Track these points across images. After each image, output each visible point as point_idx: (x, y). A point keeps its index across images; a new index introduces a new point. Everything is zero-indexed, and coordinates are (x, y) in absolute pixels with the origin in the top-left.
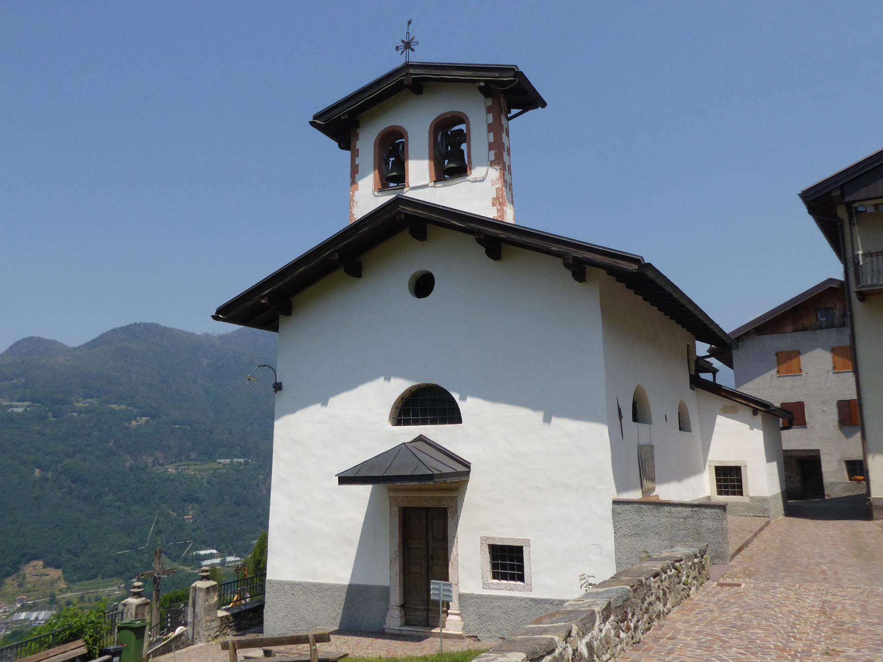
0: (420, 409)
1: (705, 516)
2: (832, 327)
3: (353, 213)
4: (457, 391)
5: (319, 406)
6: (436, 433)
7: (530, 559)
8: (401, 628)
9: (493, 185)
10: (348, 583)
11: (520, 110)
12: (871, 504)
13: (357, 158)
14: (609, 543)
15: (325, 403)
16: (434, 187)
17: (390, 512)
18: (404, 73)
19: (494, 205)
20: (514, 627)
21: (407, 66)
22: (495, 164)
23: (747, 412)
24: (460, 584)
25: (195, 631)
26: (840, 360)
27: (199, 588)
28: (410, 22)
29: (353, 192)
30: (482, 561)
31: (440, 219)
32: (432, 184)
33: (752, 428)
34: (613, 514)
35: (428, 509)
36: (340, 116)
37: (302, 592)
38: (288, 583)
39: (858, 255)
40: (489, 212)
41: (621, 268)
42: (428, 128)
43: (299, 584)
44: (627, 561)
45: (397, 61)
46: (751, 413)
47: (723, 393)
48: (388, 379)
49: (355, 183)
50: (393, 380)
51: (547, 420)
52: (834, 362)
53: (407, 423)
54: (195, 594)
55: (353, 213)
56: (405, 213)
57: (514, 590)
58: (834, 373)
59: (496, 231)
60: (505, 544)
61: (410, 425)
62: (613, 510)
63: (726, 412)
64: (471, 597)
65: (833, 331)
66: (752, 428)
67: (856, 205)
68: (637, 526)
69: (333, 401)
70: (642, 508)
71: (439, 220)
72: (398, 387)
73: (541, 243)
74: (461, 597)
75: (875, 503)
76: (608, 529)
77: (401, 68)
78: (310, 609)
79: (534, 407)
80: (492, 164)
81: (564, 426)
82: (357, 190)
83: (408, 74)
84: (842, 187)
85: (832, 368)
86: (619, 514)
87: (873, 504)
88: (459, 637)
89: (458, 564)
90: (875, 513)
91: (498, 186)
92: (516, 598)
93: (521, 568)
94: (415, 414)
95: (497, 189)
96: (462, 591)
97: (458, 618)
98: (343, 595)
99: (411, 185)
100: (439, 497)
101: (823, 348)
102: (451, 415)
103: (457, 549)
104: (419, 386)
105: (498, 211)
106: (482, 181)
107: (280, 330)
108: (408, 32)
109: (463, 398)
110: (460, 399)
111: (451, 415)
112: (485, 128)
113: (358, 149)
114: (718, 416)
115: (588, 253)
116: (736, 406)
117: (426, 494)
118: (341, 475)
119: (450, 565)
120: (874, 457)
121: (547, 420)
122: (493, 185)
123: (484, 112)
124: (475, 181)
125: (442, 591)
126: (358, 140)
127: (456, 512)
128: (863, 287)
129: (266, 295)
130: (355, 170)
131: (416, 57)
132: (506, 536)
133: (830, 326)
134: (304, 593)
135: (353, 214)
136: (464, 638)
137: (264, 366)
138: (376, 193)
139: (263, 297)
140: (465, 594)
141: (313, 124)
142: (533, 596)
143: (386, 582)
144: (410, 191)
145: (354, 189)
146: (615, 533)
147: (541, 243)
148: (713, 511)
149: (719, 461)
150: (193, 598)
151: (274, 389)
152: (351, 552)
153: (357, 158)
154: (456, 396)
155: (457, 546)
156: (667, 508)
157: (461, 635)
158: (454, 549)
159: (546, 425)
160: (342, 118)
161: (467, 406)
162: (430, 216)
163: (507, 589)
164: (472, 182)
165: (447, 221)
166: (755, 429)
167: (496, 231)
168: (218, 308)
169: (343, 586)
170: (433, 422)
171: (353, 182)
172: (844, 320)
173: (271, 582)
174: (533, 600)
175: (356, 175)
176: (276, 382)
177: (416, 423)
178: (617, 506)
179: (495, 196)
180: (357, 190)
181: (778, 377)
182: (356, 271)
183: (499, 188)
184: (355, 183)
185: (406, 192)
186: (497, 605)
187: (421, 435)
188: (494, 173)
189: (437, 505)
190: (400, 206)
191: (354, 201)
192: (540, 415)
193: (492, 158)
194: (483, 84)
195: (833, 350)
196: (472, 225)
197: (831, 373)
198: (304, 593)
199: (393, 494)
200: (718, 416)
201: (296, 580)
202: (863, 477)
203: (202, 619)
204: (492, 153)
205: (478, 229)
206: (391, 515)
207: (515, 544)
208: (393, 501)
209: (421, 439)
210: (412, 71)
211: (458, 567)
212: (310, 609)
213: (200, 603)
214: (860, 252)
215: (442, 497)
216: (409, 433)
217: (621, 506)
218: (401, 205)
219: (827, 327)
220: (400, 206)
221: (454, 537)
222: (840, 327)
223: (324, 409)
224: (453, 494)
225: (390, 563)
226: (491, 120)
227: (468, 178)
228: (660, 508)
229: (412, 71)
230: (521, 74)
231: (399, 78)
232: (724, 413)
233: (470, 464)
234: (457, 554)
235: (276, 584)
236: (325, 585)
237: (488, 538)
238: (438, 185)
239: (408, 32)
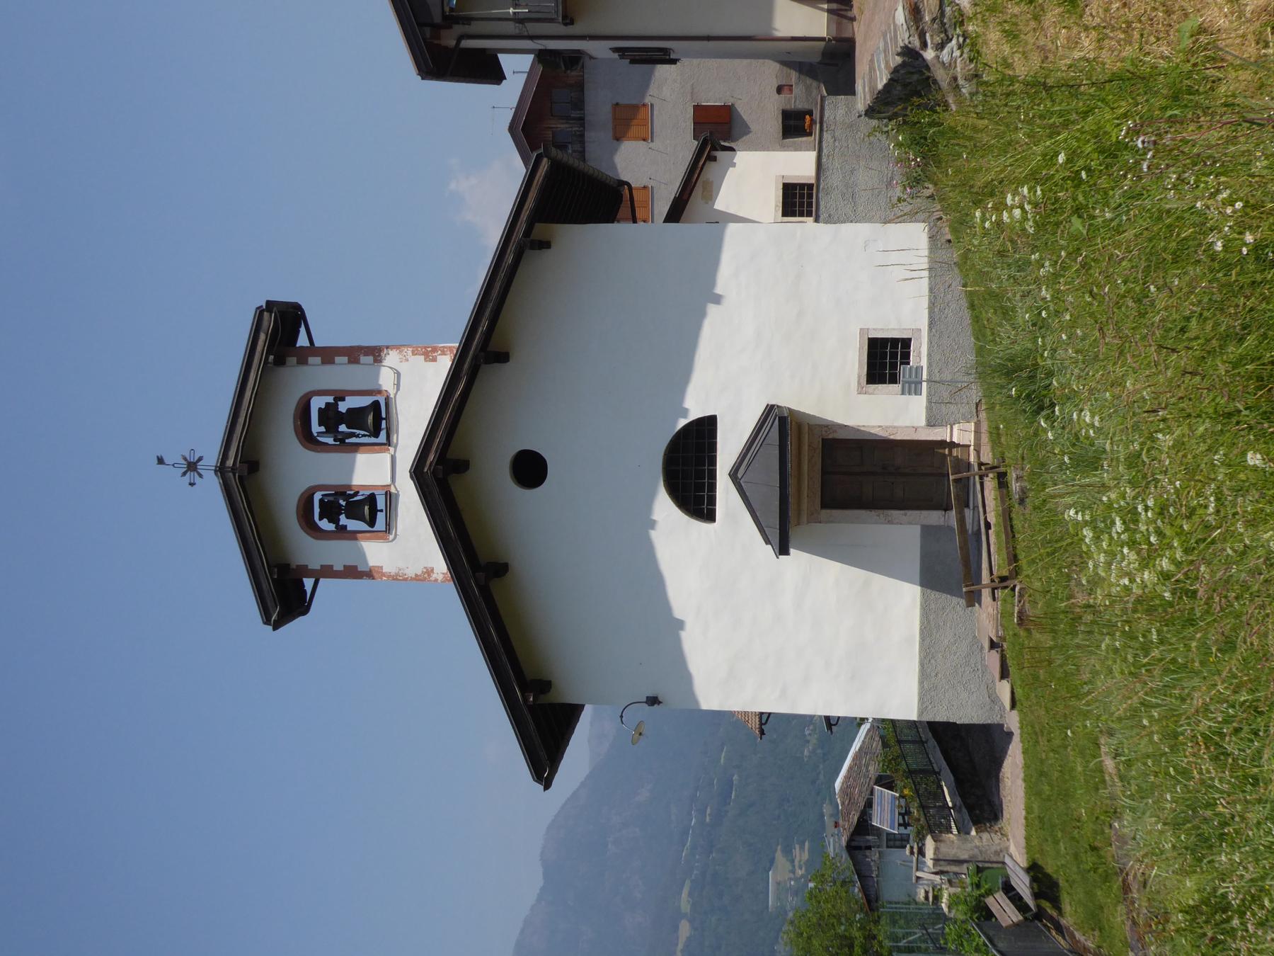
0: (695, 479)
1: (832, 118)
2: (582, 136)
3: (414, 576)
4: (675, 422)
5: (683, 634)
6: (728, 450)
7: (882, 329)
8: (971, 508)
9: (407, 360)
10: (919, 588)
11: (303, 325)
12: (835, 39)
13: (335, 569)
14: (862, 230)
15: (680, 624)
16: (396, 447)
17: (826, 522)
18: (231, 474)
19: (434, 360)
20: (962, 353)
21: (221, 470)
22: (380, 355)
23: (711, 170)
24: (915, 425)
25: (995, 860)
26: (634, 130)
27: (935, 854)
28: (161, 461)
29: (383, 574)
30: (886, 395)
31: (451, 413)
32: (392, 449)
33: (734, 165)
34: (830, 223)
35: (824, 472)
36: (273, 579)
37: (933, 661)
38: (921, 683)
39: (514, 13)
40: (445, 364)
41: (544, 180)
42: (313, 453)
43: (922, 665)
44: (883, 208)
45: (211, 485)
46: (713, 163)
47: (685, 197)
48: (652, 524)
49: (370, 571)
50: (655, 517)
51: (717, 300)
52: (636, 139)
53: (712, 501)
54: (944, 860)
55: (414, 576)
56: (436, 464)
57: (920, 352)
58: (652, 141)
59: (479, 334)
60: (866, 361)
61: (716, 470)
62: (826, 223)
63: (710, 195)
64: (929, 409)
65: (590, 135)
66: (734, 165)
67: (447, 9)
68: (843, 195)
69: (678, 613)
70: (823, 189)
71: (453, 414)
72: (665, 508)
73: (501, 275)
74: (931, 423)
75: (834, 33)
76: (847, 229)
77: (223, 479)
78: (954, 648)
79: (702, 315)
80: (378, 360)
81: (725, 279)
82: (382, 567)
83: (233, 469)
84: (420, 25)
85: (645, 143)
86: (830, 216)
87: (834, 36)
88: (978, 425)
89: (891, 427)
90: (847, 35)
91: (410, 353)
92: (929, 349)
93: (894, 342)
94: (700, 487)
95: (414, 353)
96: (923, 422)
97: (956, 427)
98: (934, 595)
99: (388, 481)
100: (809, 450)
101: (615, 150)
102: (705, 429)
103: (873, 427)
104: (664, 481)
105: (443, 353)
106: (398, 374)
107: (574, 700)
108: (173, 465)
109: (685, 412)
110: (685, 417)
111: (705, 429)
112: (328, 368)
113: (321, 566)
114: (716, 207)
115: (522, 216)
116: (704, 182)
117: (805, 467)
118: (777, 551)
119: (892, 437)
120: (776, 30)
121: (717, 300)
122: (407, 360)
123: (305, 368)
124: (398, 385)
125: (912, 380)
126: (307, 566)
127: (827, 426)
128: (557, 12)
129: (523, 695)
130: (352, 572)
131: (211, 454)
132: (855, 361)
133: (581, 138)
134: (933, 657)
135: (416, 575)
136: (979, 421)
137: (622, 717)
138: (391, 537)
139: (525, 699)
140: (926, 418)
141: (276, 626)
142: (927, 328)
143: (916, 531)
144: (396, 484)
145: (378, 572)
146: (851, 222)
147: (501, 275)
148: (826, 108)
149: (776, 211)
150: (949, 864)
151: (656, 706)
152: (879, 581)
153: (335, 569)
154: (682, 423)
155: (868, 426)
156: (824, 160)
157: (975, 423)
158: (873, 431)
159: (725, 302)
160: (276, 577)
161: (695, 409)
162: (445, 428)
163: (920, 355)
164: (398, 389)
165: (456, 401)
166: (735, 161)
167: (479, 334)
168: (534, 780)
169: (923, 594)
170: (713, 461)
171: (369, 574)
172: (574, 119)
173: (921, 713)
174: (930, 328)
175: (359, 570)
176: (646, 702)
177: (712, 487)
178: (822, 217)
179: (423, 357)
180: (382, 567)
181: (652, 222)
182: (501, 569)
183: (413, 352)
184: (370, 571)
185: (397, 490)
186: (938, 375)
187: (729, 474)
188: (391, 358)
189: (819, 451)
190: (426, 470)
191: (397, 575)
192: (712, 309)
193: (370, 359)
194: (271, 357)
195: (618, 138)
196: (466, 366)
197: (651, 145)
198: (933, 657)
199: (804, 518)
200: (716, 207)
201: (917, 670)
202: (807, 117)
203: (977, 847)
204: (363, 359)
205: (472, 360)
206: (832, 522)
207: (866, 347)
208: (813, 519)
209: (734, 475)
210: (230, 463)
211: (895, 427)
212: (954, 648)
213: (954, 851)
214: (511, 10)
215: (809, 446)
216: (726, 494)
217: (821, 212)
218: (423, 468)
219: (583, 143)
220: (426, 470)
221: (858, 430)
222: (583, 125)
223: (688, 626)
224: (806, 429)
225: (892, 524)
226: (318, 360)
227: (392, 396)
228: (824, 167)
229: (230, 463)
230: (270, 304)
231: (234, 483)
232: (711, 200)
233: (768, 405)
234: (879, 427)
235: (923, 703)
236: (922, 623)
237: (859, 383)
238: (395, 441)
239: (173, 465)
